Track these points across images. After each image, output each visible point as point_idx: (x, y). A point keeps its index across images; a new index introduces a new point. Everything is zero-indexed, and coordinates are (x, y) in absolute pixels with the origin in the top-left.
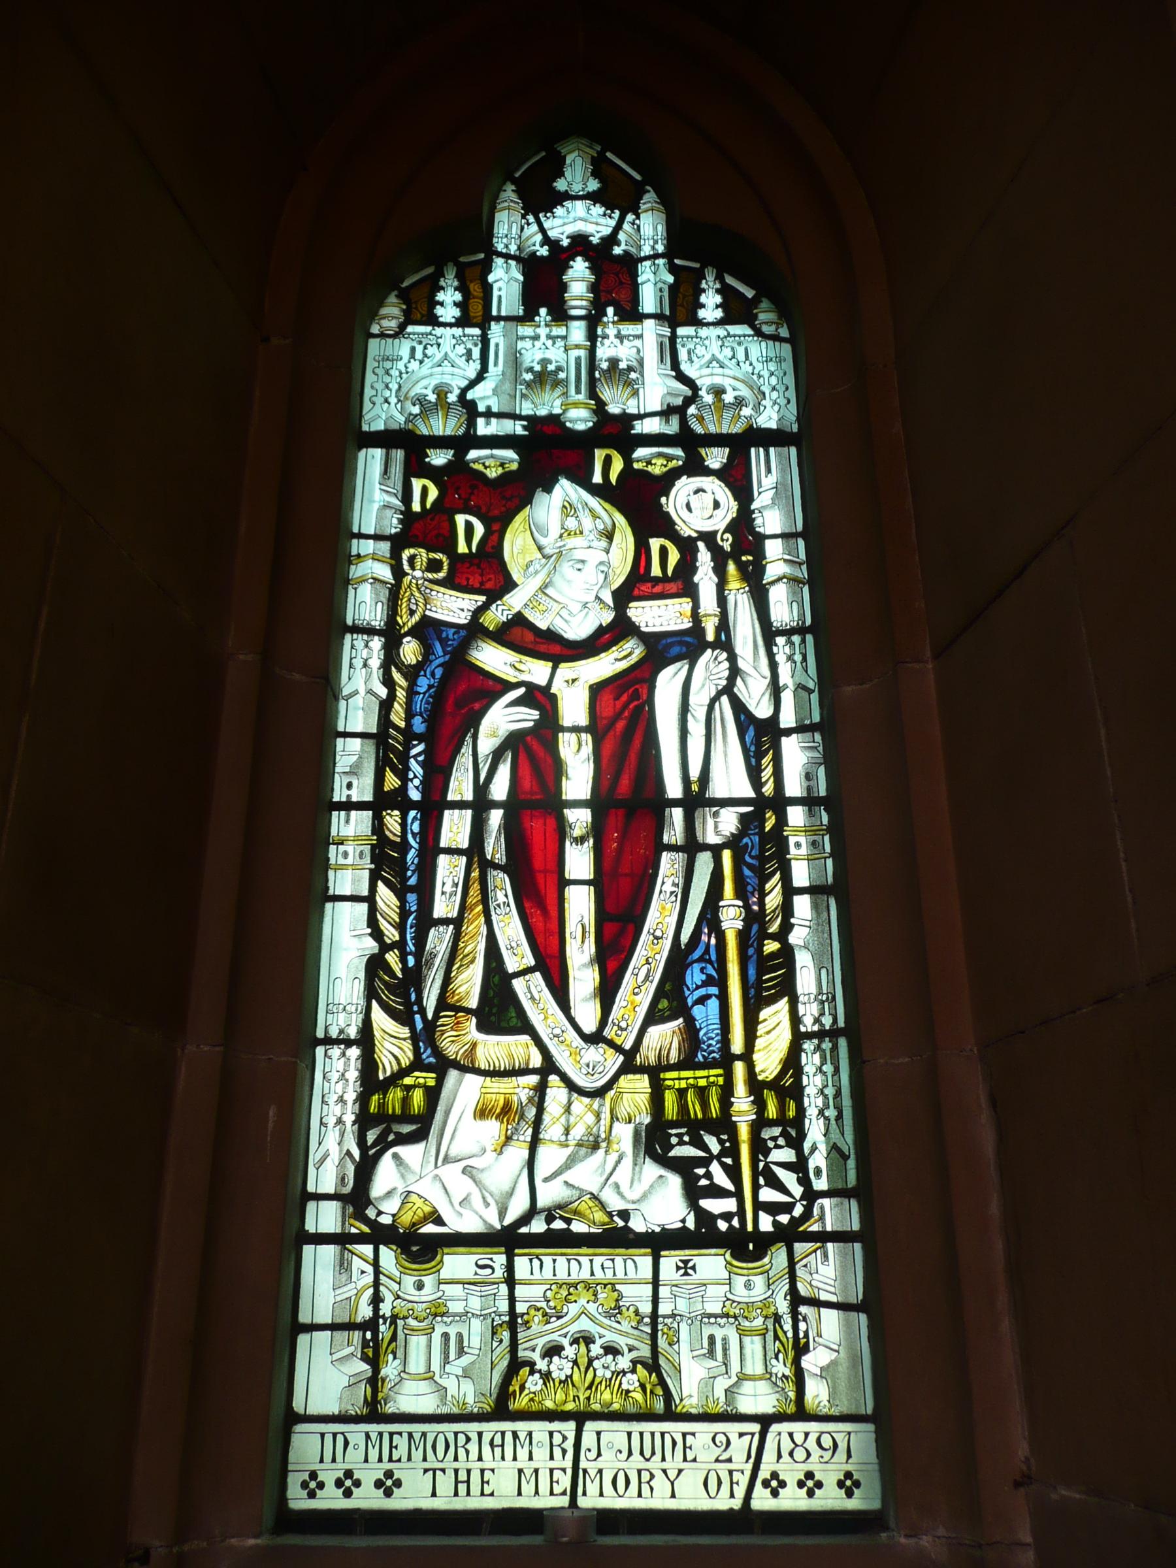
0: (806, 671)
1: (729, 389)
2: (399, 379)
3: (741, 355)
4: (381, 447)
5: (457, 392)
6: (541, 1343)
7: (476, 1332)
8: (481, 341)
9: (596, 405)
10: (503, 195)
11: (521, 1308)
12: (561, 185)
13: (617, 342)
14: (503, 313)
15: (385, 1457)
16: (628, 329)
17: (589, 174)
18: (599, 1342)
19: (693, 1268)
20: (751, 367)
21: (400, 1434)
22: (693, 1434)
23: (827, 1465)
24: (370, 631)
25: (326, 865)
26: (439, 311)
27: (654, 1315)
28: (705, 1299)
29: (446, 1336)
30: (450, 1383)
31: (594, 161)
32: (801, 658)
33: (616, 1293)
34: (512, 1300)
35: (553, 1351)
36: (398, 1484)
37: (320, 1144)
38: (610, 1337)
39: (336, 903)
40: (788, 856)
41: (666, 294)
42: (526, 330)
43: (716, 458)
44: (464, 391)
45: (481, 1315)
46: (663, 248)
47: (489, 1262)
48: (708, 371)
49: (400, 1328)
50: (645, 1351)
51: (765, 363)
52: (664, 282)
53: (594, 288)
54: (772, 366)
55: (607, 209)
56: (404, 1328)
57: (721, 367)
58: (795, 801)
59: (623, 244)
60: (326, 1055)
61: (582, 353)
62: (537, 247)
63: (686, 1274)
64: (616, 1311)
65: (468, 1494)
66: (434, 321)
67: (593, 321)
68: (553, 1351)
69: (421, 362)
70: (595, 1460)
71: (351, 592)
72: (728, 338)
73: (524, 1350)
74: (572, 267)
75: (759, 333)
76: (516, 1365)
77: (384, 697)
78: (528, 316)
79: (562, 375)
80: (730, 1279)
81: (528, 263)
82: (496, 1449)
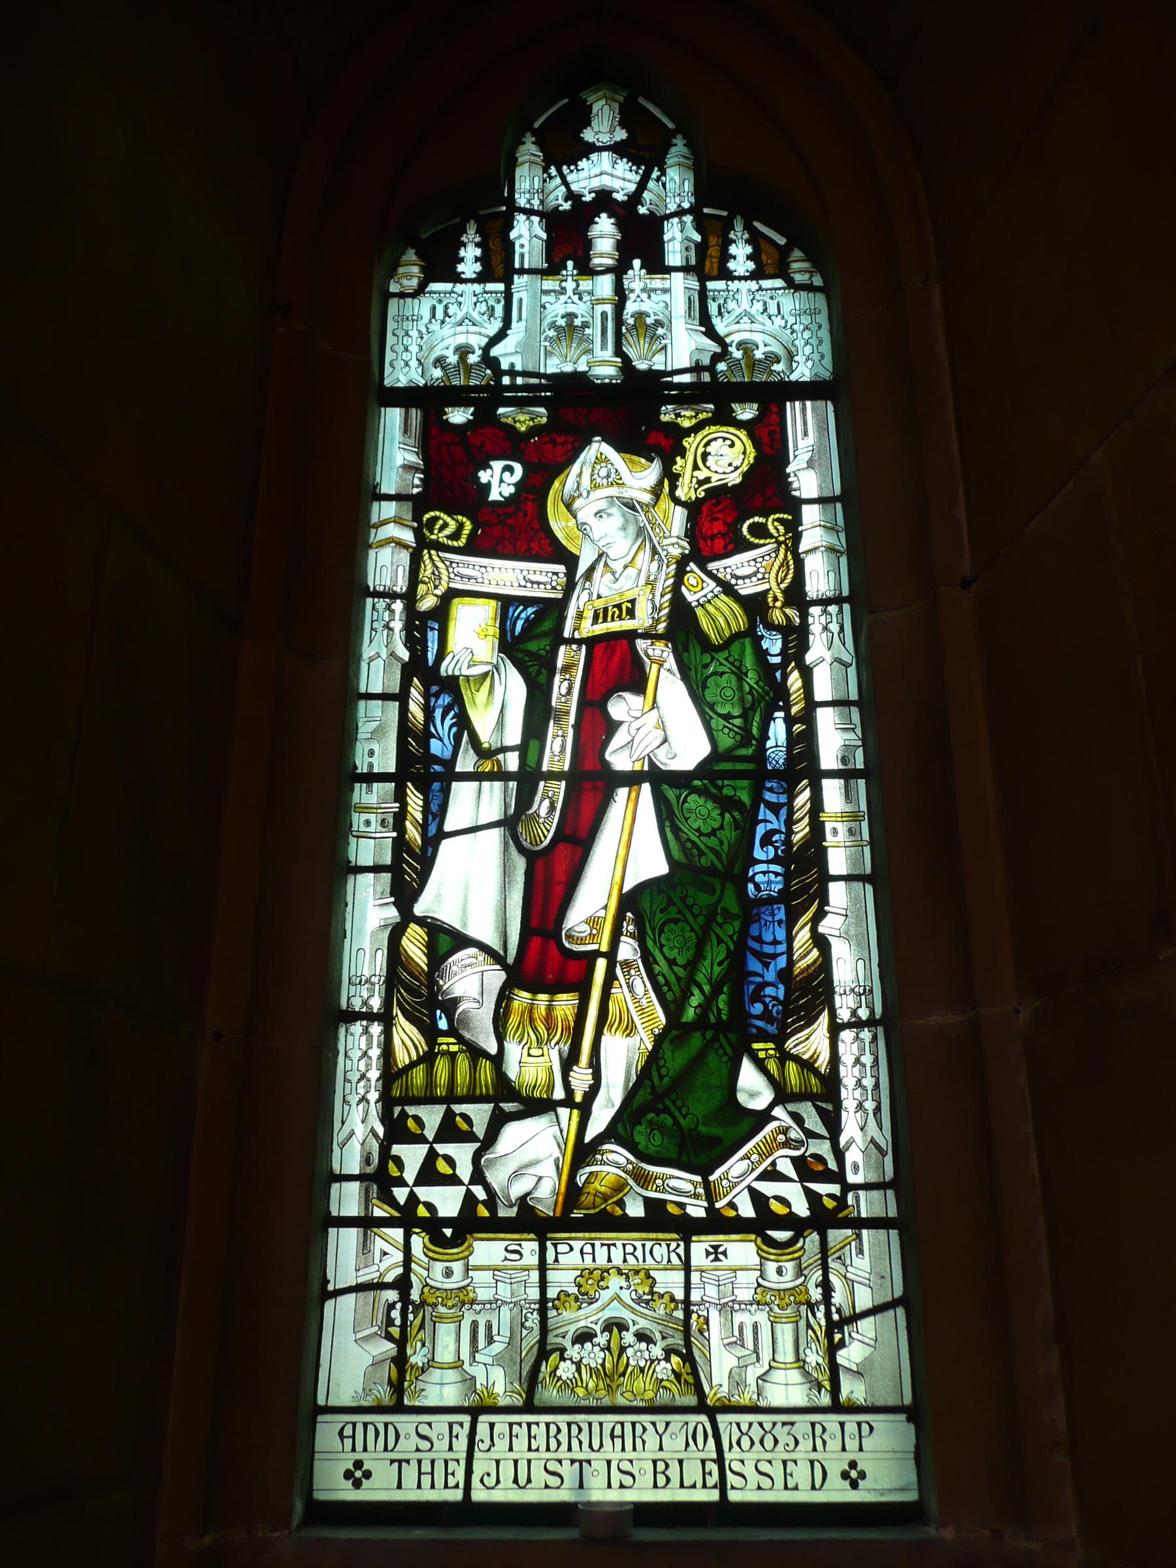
0: (844, 645)
1: (761, 345)
2: (419, 340)
3: (773, 309)
4: (400, 407)
5: (479, 352)
6: (572, 1329)
8: (505, 298)
9: (622, 363)
10: (522, 148)
11: (552, 1293)
12: (588, 135)
13: (644, 296)
14: (526, 266)
16: (657, 282)
17: (617, 123)
18: (633, 1329)
19: (724, 1253)
20: (783, 321)
23: (621, 1458)
24: (393, 596)
26: (460, 268)
27: (687, 1302)
28: (734, 1286)
29: (475, 1325)
30: (478, 1372)
32: (838, 629)
33: (651, 1280)
34: (543, 1284)
35: (584, 1337)
36: (368, 1475)
38: (642, 1323)
40: (824, 844)
42: (550, 284)
43: (746, 412)
44: (486, 349)
45: (511, 1302)
47: (517, 1248)
48: (737, 327)
49: (428, 1317)
50: (678, 1341)
51: (798, 317)
53: (620, 246)
54: (806, 320)
56: (432, 1316)
61: (609, 308)
62: (561, 201)
63: (717, 1259)
65: (433, 1486)
66: (457, 278)
67: (619, 270)
68: (584, 1337)
69: (443, 322)
70: (489, 1450)
72: (760, 292)
73: (556, 1336)
74: (597, 223)
75: (792, 285)
76: (543, 1352)
78: (553, 268)
81: (551, 218)
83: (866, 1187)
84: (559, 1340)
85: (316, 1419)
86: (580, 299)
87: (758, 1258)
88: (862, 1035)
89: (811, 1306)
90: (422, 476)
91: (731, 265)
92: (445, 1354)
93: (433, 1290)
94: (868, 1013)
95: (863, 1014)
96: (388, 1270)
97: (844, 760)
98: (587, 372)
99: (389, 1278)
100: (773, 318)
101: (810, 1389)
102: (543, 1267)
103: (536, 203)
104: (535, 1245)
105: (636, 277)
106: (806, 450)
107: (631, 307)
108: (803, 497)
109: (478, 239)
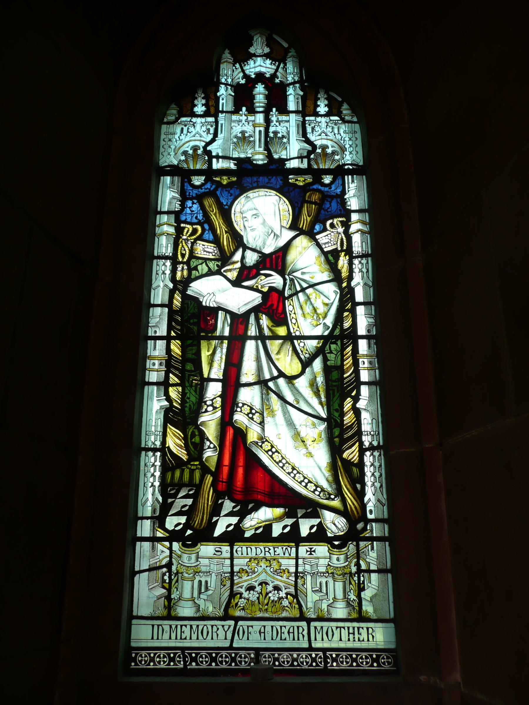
3: (336, 131)
5: (202, 149)
6: (245, 584)
7: (213, 581)
9: (267, 153)
10: (224, 56)
11: (236, 569)
12: (252, 50)
13: (277, 124)
15: (179, 637)
16: (284, 118)
21: (186, 626)
22: (252, 626)
24: (166, 258)
25: (144, 369)
26: (196, 109)
29: (200, 582)
30: (201, 603)
31: (267, 40)
35: (251, 588)
37: (144, 495)
39: (154, 308)
41: (300, 101)
42: (234, 117)
44: (205, 148)
46: (298, 78)
48: (320, 137)
49: (180, 578)
50: (292, 590)
52: (299, 95)
53: (267, 97)
55: (272, 61)
56: (182, 577)
57: (326, 135)
58: (362, 337)
59: (280, 78)
60: (146, 455)
61: (262, 129)
62: (241, 80)
64: (280, 571)
68: (251, 588)
69: (187, 135)
71: (156, 239)
73: (238, 588)
75: (344, 121)
76: (232, 595)
77: (172, 288)
78: (236, 111)
79: (252, 139)
80: (330, 556)
81: (237, 88)
82: (290, 634)
83: (376, 520)
84: (240, 589)
85: (131, 622)
86: (248, 124)
87: (329, 554)
88: (374, 454)
89: (351, 574)
90: (180, 203)
91: (318, 109)
92: (187, 594)
93: (182, 566)
94: (377, 443)
95: (375, 443)
96: (163, 559)
97: (369, 331)
98: (251, 157)
99: (164, 563)
100: (336, 135)
101: (350, 610)
102: (232, 558)
103: (229, 80)
104: (228, 548)
105: (274, 116)
106: (354, 188)
107: (272, 129)
108: (352, 209)
109: (203, 96)
